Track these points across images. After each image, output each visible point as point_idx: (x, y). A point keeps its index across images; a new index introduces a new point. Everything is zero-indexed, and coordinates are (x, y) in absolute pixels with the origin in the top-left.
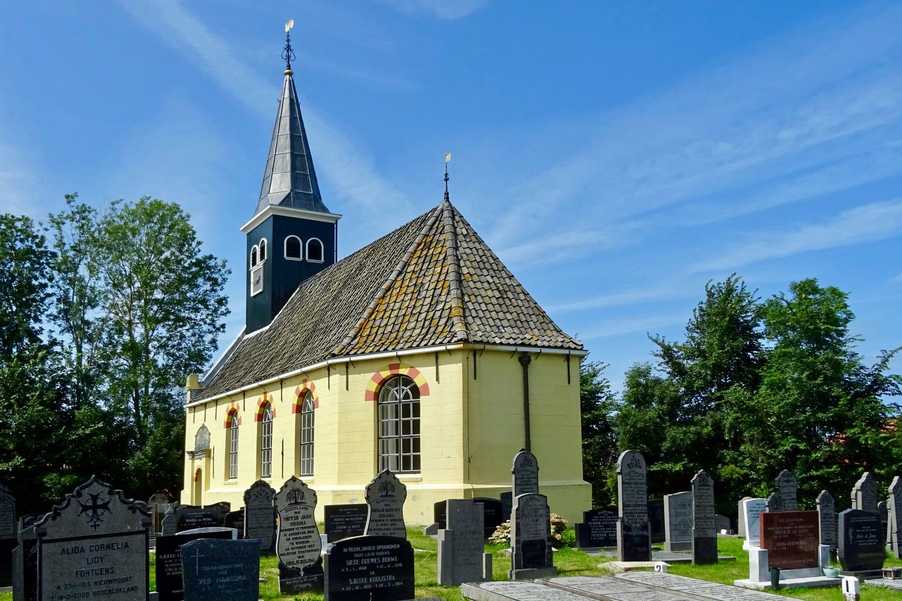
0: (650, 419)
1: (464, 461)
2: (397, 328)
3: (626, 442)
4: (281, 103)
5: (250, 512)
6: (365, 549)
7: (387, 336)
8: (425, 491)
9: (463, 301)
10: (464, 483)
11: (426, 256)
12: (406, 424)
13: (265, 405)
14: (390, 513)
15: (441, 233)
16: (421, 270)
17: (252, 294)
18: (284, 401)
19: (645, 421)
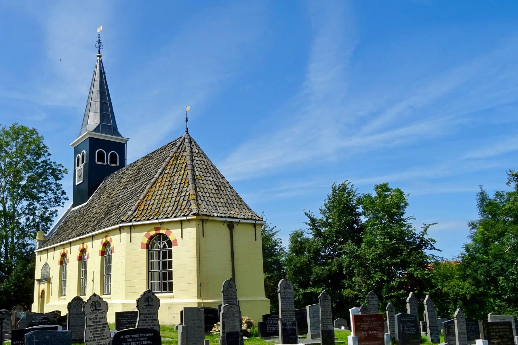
0: (304, 261)
1: (198, 285)
2: (159, 206)
3: (291, 275)
4: (95, 72)
5: (71, 316)
6: (133, 336)
7: (153, 210)
8: (177, 304)
9: (196, 191)
10: (198, 299)
11: (176, 164)
13: (83, 251)
14: (150, 315)
15: (184, 151)
16: (173, 172)
17: (77, 184)
18: (94, 248)
19: (301, 263)
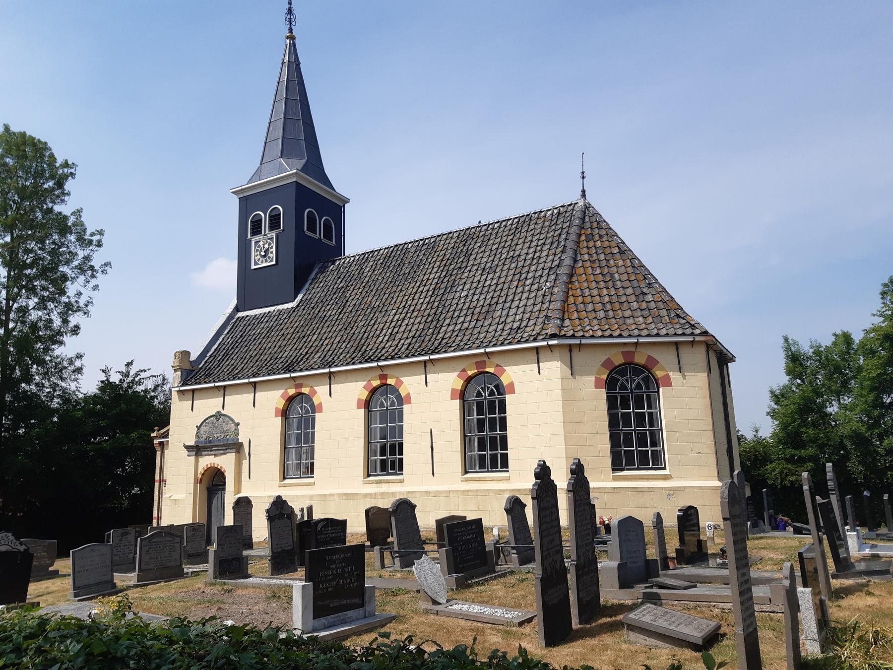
12: (492, 421)
